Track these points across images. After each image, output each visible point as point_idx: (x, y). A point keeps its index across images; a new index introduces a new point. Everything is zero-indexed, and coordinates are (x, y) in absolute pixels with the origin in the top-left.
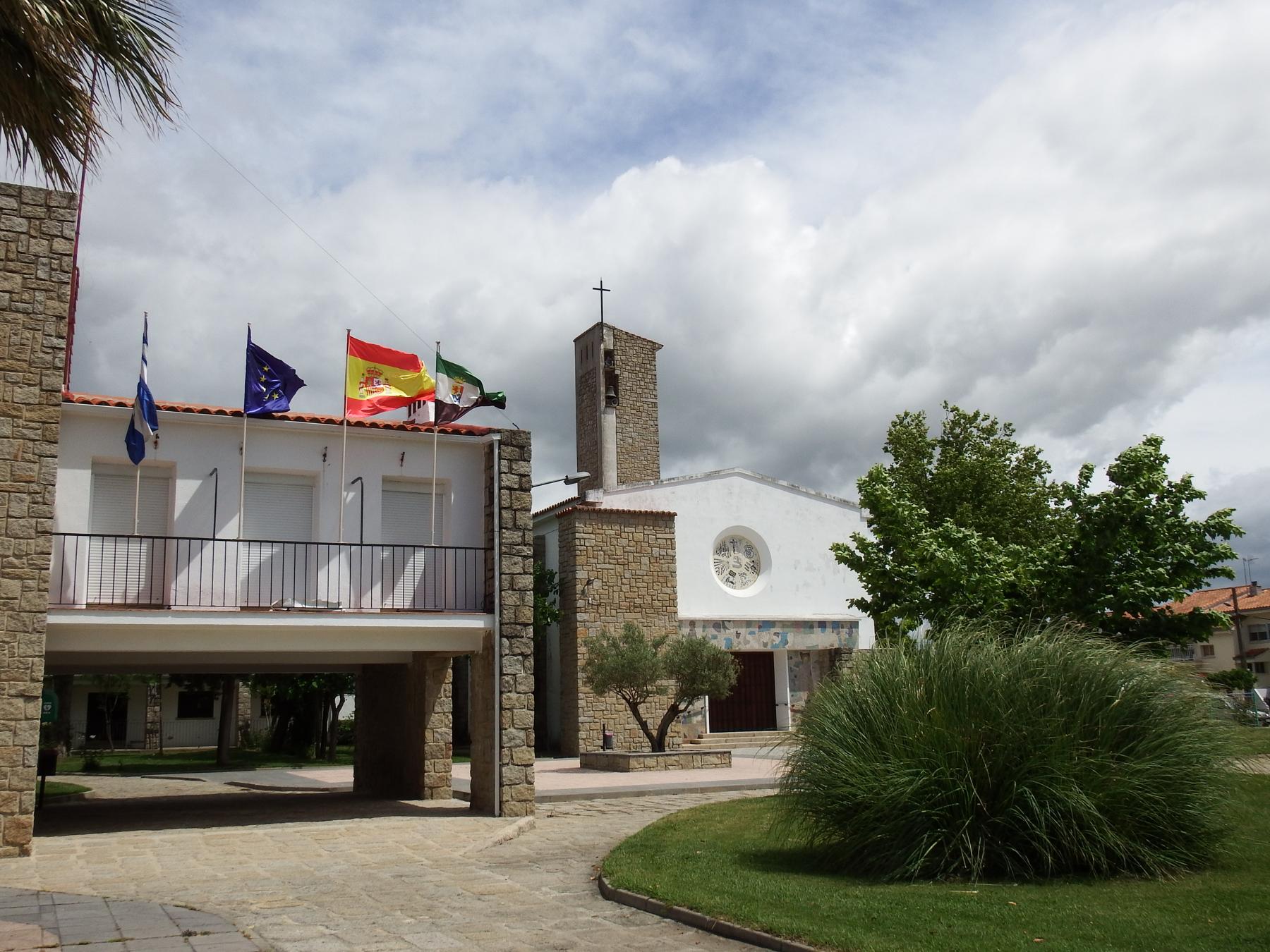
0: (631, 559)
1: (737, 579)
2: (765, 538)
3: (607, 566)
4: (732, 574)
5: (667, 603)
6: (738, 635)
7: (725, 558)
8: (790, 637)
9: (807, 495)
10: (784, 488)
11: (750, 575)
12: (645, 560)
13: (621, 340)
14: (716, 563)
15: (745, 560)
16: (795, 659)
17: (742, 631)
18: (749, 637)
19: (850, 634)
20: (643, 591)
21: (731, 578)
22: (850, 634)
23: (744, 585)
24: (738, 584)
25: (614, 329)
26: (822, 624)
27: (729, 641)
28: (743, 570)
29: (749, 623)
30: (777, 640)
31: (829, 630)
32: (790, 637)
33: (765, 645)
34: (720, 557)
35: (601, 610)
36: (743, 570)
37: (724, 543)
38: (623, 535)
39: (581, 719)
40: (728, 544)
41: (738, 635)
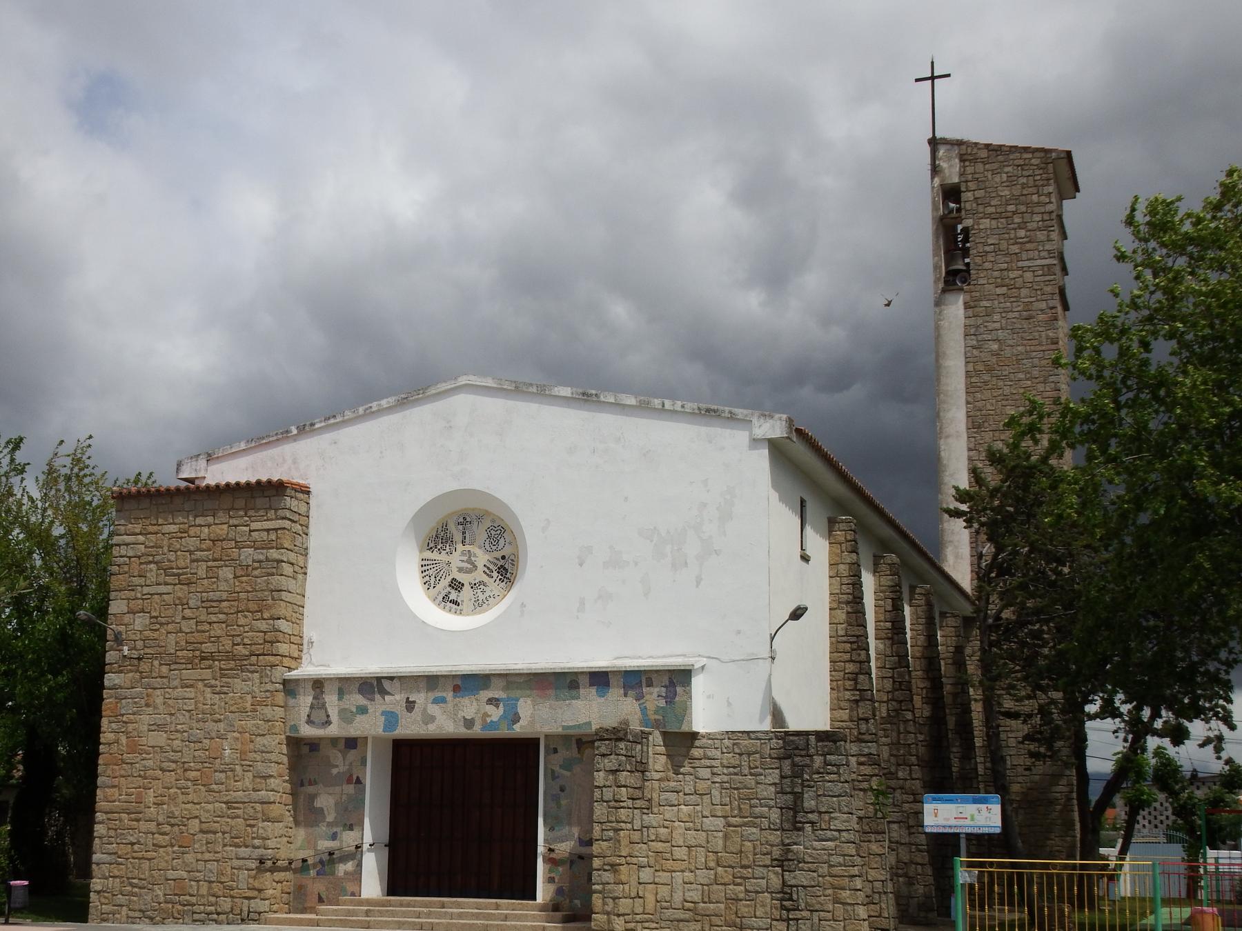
0: (202, 572)
1: (466, 594)
2: (516, 508)
3: (163, 589)
4: (456, 585)
5: (258, 649)
6: (410, 705)
7: (443, 557)
8: (525, 708)
9: (619, 407)
10: (567, 401)
11: (494, 586)
12: (227, 573)
13: (975, 160)
14: (425, 567)
15: (482, 558)
16: (563, 754)
17: (420, 698)
18: (434, 710)
19: (670, 698)
20: (218, 630)
21: (451, 595)
22: (670, 698)
23: (479, 605)
24: (467, 605)
25: (959, 143)
26: (600, 679)
27: (391, 720)
28: (479, 575)
29: (431, 681)
30: (495, 713)
31: (615, 693)
32: (525, 708)
33: (469, 723)
34: (434, 555)
35: (144, 666)
36: (479, 575)
37: (445, 527)
38: (192, 531)
39: (95, 857)
40: (452, 527)
41: (410, 705)
